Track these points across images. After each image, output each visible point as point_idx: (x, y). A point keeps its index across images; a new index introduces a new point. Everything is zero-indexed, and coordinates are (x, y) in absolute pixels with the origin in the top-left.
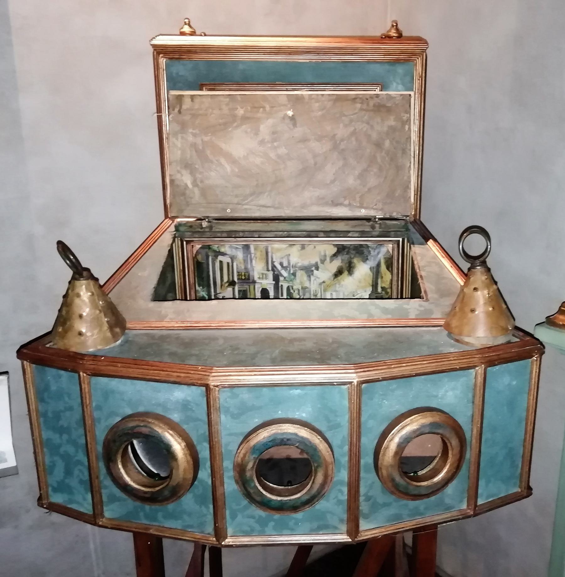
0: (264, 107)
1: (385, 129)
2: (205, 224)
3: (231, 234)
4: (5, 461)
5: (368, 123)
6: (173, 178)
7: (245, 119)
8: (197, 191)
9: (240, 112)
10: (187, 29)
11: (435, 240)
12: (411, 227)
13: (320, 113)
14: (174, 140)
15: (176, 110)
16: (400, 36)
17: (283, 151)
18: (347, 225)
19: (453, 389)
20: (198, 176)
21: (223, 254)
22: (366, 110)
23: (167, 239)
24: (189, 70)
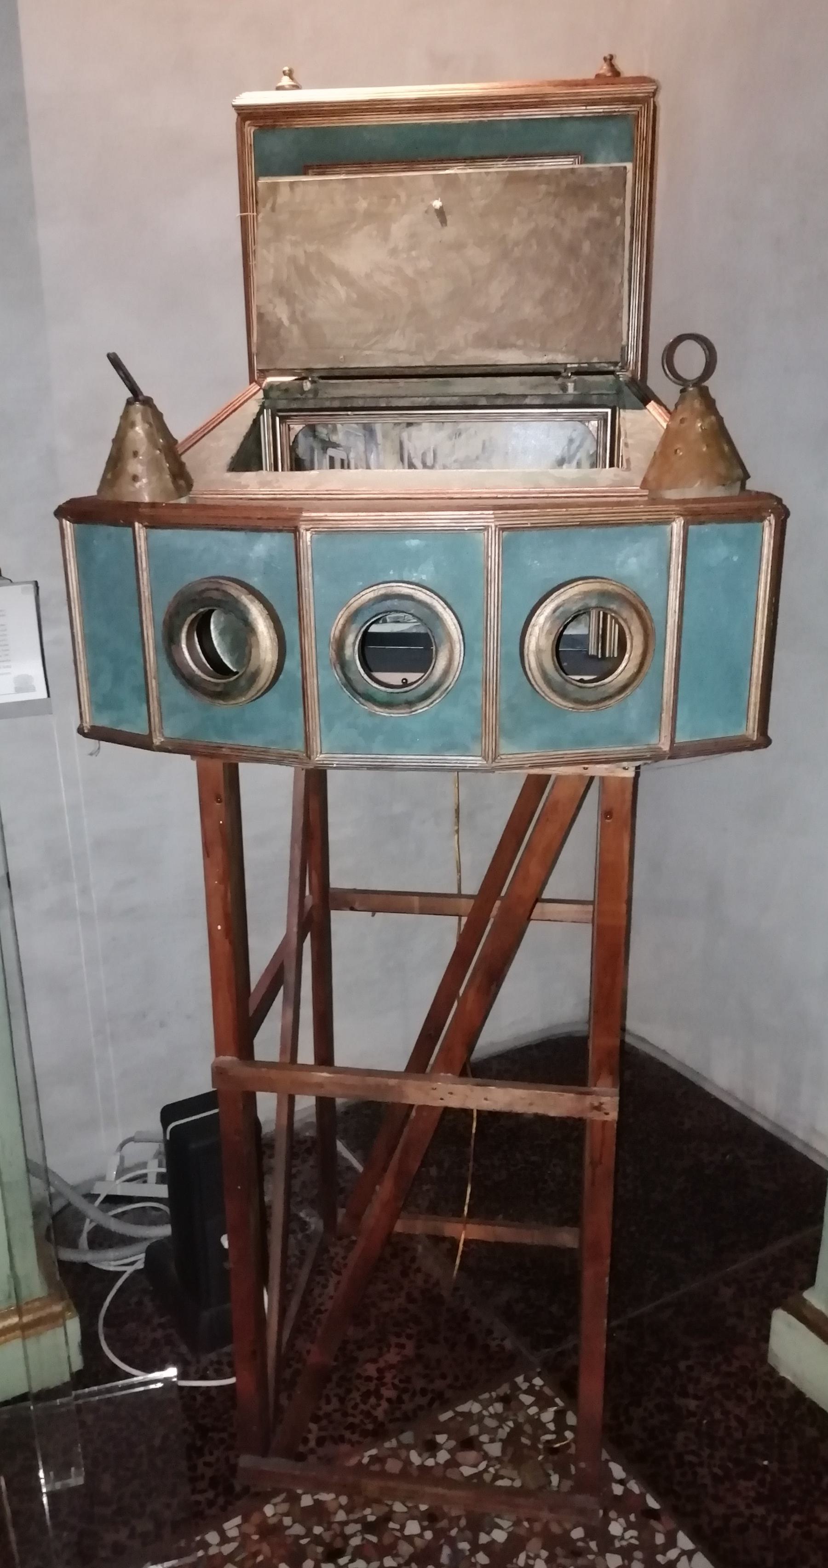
0: (398, 197)
1: (584, 224)
2: (307, 385)
3: (347, 407)
4: (33, 689)
5: (557, 216)
6: (262, 311)
7: (370, 216)
8: (296, 330)
9: (363, 205)
10: (286, 81)
11: (659, 402)
12: (626, 389)
13: (483, 202)
14: (265, 252)
15: (269, 206)
16: (616, 73)
17: (425, 264)
18: (522, 384)
19: (637, 555)
20: (299, 307)
21: (335, 445)
22: (555, 195)
23: (252, 407)
24: (287, 144)
